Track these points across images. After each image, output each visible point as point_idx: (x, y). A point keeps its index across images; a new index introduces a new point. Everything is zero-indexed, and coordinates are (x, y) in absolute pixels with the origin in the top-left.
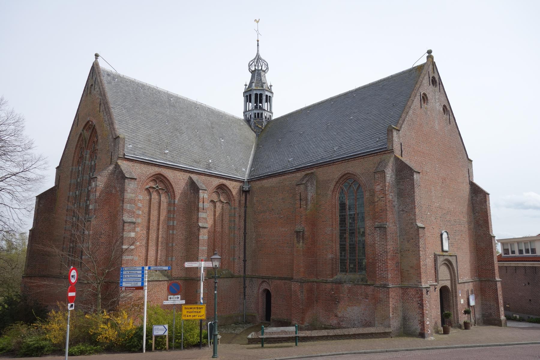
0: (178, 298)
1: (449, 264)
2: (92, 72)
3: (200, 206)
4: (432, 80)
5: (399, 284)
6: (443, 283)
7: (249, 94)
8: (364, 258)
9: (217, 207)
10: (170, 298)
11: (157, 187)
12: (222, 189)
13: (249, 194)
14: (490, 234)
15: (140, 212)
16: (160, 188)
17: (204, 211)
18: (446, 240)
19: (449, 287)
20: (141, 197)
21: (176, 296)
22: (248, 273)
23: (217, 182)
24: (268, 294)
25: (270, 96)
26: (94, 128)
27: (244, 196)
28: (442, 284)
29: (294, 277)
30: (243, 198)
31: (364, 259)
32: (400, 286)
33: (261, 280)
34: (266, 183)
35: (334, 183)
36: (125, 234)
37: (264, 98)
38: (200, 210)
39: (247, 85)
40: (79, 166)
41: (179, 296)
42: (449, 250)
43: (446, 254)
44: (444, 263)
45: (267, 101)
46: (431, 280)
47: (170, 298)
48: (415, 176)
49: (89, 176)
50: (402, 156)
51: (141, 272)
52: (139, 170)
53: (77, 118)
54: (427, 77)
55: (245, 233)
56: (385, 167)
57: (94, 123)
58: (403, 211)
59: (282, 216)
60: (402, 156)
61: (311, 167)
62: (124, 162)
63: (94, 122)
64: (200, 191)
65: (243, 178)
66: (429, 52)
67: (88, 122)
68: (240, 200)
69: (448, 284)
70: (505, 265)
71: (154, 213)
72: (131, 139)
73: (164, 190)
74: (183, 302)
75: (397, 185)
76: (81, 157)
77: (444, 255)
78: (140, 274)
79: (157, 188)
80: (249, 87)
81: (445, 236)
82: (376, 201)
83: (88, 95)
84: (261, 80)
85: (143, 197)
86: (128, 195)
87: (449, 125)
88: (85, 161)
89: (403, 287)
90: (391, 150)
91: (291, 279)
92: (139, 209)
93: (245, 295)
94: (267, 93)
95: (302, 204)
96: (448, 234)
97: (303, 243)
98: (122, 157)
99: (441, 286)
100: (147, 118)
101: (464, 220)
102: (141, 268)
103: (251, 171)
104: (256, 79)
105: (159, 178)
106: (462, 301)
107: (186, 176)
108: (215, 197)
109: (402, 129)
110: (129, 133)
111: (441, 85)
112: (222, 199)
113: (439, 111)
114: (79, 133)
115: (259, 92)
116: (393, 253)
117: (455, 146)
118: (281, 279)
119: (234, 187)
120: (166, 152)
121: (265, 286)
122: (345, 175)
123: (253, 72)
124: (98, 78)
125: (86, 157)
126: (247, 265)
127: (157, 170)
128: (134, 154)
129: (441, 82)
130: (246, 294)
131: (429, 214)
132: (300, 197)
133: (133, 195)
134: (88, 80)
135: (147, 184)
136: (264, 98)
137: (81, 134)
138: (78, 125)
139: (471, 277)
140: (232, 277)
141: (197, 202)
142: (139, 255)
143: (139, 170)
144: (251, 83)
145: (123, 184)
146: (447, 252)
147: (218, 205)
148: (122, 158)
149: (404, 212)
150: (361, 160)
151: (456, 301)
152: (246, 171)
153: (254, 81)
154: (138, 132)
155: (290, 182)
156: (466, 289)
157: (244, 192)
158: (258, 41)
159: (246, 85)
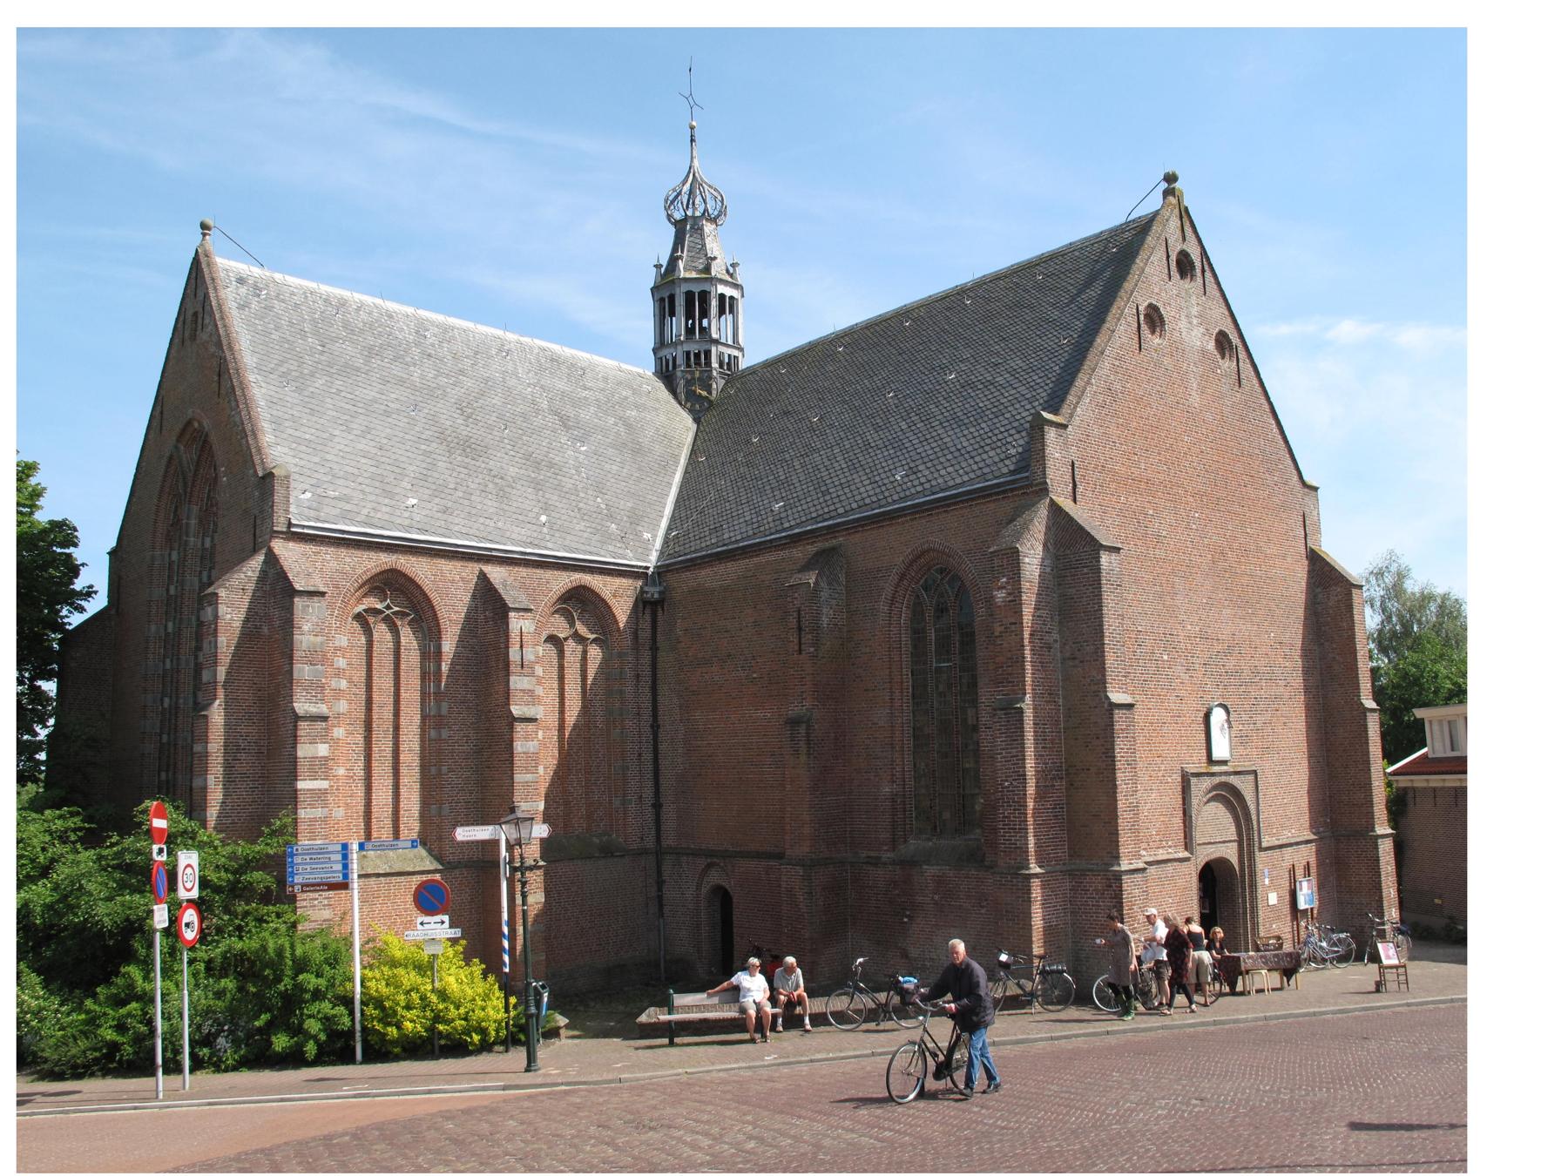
0: (443, 922)
1: (1229, 797)
2: (194, 275)
3: (511, 658)
4: (1178, 262)
5: (1064, 864)
6: (1212, 853)
7: (668, 294)
8: (977, 791)
9: (567, 654)
10: (422, 924)
11: (388, 607)
12: (580, 602)
13: (663, 610)
14: (1362, 704)
15: (344, 684)
16: (397, 609)
17: (526, 670)
18: (1222, 729)
19: (1234, 861)
20: (342, 641)
21: (438, 918)
22: (669, 840)
23: (562, 582)
24: (723, 898)
25: (732, 298)
26: (205, 441)
27: (648, 617)
28: (1208, 855)
29: (788, 852)
30: (646, 624)
31: (977, 794)
32: (1064, 868)
33: (702, 862)
34: (707, 577)
35: (893, 578)
36: (303, 751)
37: (714, 303)
38: (512, 668)
39: (662, 266)
40: (171, 549)
41: (446, 918)
42: (1232, 755)
43: (1224, 768)
44: (1217, 795)
45: (722, 312)
46: (1170, 847)
47: (422, 924)
48: (1105, 559)
49: (200, 581)
50: (1075, 501)
51: (339, 857)
52: (334, 564)
53: (159, 408)
54: (1160, 253)
55: (655, 727)
56: (1018, 536)
57: (206, 429)
58: (1074, 659)
59: (755, 675)
60: (1075, 501)
61: (832, 530)
62: (291, 544)
63: (205, 424)
64: (512, 614)
65: (644, 564)
66: (1171, 178)
67: (189, 423)
68: (637, 630)
69: (1231, 853)
70: (1448, 784)
71: (383, 682)
72: (309, 473)
73: (408, 615)
74: (455, 933)
75: (1060, 585)
76: (176, 523)
77: (1213, 774)
78: (336, 862)
79: (387, 612)
80: (666, 269)
81: (1218, 716)
82: (997, 634)
83: (188, 343)
84: (704, 245)
85: (347, 638)
86: (305, 637)
87: (1236, 388)
88: (187, 536)
89: (1073, 870)
90: (1041, 484)
91: (780, 856)
92: (339, 673)
93: (661, 906)
94: (721, 289)
95: (803, 641)
96: (1228, 712)
97: (809, 754)
98: (284, 530)
99: (1207, 859)
100: (353, 402)
101: (1287, 664)
102: (339, 848)
103: (666, 541)
104: (688, 246)
105: (391, 584)
106: (1273, 899)
107: (471, 571)
108: (560, 627)
109: (1076, 421)
110: (302, 456)
111: (1208, 274)
112: (582, 629)
113: (1203, 352)
114: (167, 455)
115: (696, 289)
116: (1046, 780)
117: (1257, 451)
118: (759, 855)
119: (620, 598)
120: (408, 502)
121: (715, 878)
122: (923, 553)
123: (680, 226)
124: (212, 295)
125: (187, 524)
126: (664, 817)
127: (385, 560)
128: (318, 520)
129: (1210, 265)
130: (664, 902)
131: (1165, 657)
132: (799, 622)
133: (319, 639)
134: (183, 299)
135: (359, 601)
136: (714, 303)
137: (171, 458)
138: (161, 429)
139: (1312, 827)
140: (608, 851)
141: (502, 646)
142: (347, 804)
143: (334, 564)
144: (673, 260)
145: (290, 609)
146: (1224, 762)
147: (570, 646)
148: (282, 533)
149: (1077, 662)
150: (964, 510)
151: (1254, 899)
152: (654, 541)
153: (682, 252)
154: (327, 449)
155: (776, 576)
156: (1287, 864)
157: (643, 604)
158: (692, 128)
159: (658, 266)
